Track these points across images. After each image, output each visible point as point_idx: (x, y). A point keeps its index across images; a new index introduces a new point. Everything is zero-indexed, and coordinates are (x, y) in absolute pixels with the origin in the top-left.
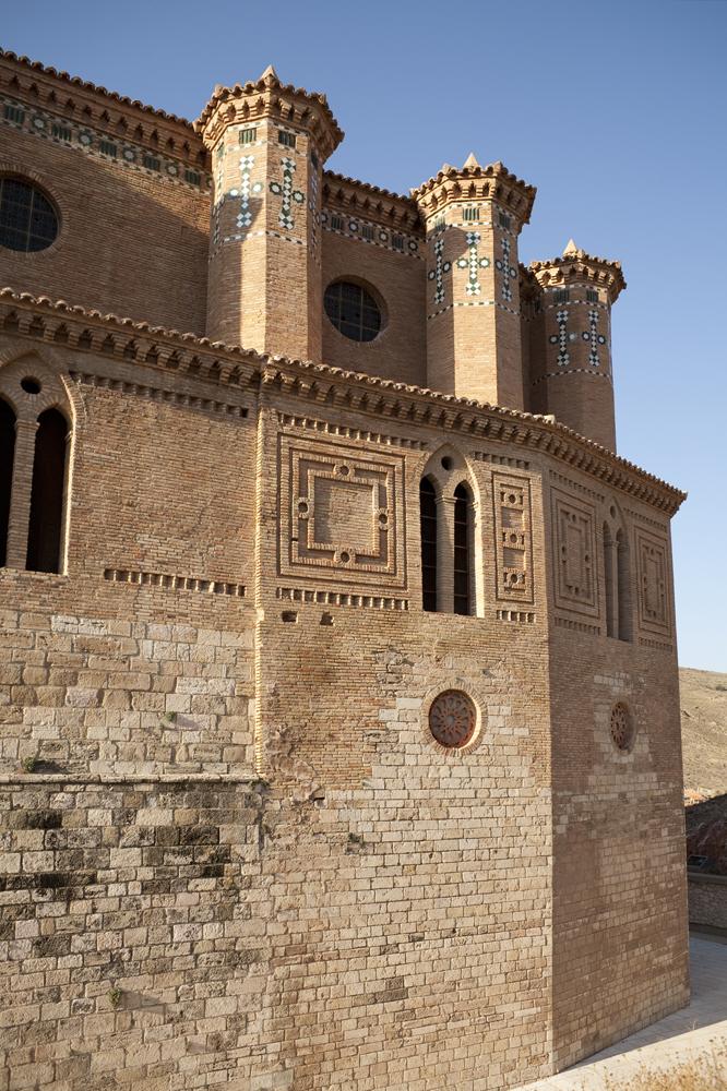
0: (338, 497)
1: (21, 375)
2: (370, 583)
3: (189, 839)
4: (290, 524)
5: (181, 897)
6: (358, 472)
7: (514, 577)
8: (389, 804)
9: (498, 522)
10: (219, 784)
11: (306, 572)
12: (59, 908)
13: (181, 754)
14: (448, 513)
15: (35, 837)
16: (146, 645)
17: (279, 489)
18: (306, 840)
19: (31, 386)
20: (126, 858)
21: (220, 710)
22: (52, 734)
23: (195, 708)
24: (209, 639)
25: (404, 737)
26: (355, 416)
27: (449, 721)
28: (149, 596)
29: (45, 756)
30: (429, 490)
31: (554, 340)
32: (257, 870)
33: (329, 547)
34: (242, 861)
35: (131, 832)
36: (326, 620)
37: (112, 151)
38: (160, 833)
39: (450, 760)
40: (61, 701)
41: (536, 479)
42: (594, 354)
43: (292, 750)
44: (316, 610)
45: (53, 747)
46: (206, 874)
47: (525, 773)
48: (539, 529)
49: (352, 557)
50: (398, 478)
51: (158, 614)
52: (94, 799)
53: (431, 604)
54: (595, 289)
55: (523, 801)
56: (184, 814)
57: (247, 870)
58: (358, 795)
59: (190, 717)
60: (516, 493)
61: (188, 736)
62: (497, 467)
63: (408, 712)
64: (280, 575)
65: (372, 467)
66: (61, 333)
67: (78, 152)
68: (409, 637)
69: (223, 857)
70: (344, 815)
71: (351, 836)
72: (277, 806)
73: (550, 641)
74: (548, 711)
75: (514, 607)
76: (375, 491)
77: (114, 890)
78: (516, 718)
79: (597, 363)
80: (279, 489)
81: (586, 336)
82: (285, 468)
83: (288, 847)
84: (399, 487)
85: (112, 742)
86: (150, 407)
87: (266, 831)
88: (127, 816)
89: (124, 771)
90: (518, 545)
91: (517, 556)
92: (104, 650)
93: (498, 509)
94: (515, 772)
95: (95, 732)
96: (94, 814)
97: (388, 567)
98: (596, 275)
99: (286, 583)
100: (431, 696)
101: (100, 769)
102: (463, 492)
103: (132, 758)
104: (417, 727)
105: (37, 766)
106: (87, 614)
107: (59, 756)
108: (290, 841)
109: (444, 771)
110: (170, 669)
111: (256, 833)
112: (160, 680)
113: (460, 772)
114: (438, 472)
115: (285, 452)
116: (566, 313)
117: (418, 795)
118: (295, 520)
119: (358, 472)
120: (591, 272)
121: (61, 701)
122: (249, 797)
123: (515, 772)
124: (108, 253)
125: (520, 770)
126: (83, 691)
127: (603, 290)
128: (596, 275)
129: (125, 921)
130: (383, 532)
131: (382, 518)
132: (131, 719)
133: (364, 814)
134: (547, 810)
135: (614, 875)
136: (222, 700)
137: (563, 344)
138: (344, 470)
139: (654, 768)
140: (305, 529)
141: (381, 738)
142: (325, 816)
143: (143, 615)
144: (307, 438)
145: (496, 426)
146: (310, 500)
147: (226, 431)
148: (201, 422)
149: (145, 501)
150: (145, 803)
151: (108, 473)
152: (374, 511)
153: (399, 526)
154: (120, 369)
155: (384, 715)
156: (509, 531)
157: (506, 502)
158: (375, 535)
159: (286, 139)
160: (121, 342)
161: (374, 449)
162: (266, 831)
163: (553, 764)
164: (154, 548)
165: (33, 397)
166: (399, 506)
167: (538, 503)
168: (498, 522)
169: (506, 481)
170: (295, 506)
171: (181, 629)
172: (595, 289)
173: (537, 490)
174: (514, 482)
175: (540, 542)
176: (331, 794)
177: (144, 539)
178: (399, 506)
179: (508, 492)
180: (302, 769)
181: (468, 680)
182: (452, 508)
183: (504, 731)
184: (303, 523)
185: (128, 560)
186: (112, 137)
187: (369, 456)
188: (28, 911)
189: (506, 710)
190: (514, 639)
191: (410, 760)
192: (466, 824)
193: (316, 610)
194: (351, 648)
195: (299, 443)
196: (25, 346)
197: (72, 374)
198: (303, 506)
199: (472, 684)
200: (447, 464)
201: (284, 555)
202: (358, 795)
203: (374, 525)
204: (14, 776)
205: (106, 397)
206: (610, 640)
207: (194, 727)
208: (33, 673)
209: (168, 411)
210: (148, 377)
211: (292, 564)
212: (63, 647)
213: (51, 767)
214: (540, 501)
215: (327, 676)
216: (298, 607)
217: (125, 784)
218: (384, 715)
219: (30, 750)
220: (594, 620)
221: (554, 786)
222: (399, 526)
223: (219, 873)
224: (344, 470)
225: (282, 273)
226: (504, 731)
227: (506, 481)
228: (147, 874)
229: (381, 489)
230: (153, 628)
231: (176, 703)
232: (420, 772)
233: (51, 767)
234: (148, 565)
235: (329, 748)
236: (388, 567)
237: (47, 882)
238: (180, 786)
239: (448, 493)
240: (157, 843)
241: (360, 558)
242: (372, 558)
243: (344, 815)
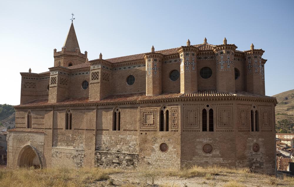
0: (148, 116)
2: (152, 128)
3: (130, 160)
5: (130, 167)
7: (175, 125)
8: (154, 159)
9: (172, 116)
11: (144, 127)
13: (131, 151)
14: (165, 115)
15: (117, 159)
16: (127, 138)
20: (124, 162)
21: (135, 146)
22: (119, 148)
23: (132, 145)
25: (156, 150)
26: (150, 104)
27: (163, 148)
28: (128, 132)
29: (119, 150)
30: (162, 113)
31: (224, 62)
32: (137, 165)
33: (147, 124)
34: (136, 164)
35: (125, 159)
36: (146, 134)
37: (139, 66)
38: (128, 159)
40: (120, 144)
41: (179, 107)
42: (229, 66)
45: (119, 149)
46: (132, 165)
47: (176, 156)
48: (180, 115)
51: (129, 134)
52: (122, 155)
53: (162, 129)
54: (222, 51)
55: (175, 161)
57: (136, 165)
58: (149, 157)
59: (131, 146)
60: (175, 110)
61: (132, 149)
63: (157, 146)
64: (140, 128)
65: (152, 111)
67: (136, 69)
68: (157, 135)
69: (134, 163)
70: (148, 160)
71: (148, 163)
72: (140, 158)
73: (181, 135)
74: (180, 146)
75: (174, 129)
77: (124, 165)
78: (174, 148)
79: (229, 68)
81: (227, 62)
84: (156, 113)
86: (127, 110)
87: (138, 161)
88: (124, 157)
89: (125, 152)
90: (176, 119)
91: (176, 121)
93: (172, 114)
94: (174, 156)
96: (122, 157)
98: (221, 48)
99: (141, 129)
100: (160, 144)
101: (123, 152)
102: (167, 111)
104: (158, 148)
105: (118, 151)
106: (122, 135)
108: (141, 162)
109: (162, 155)
110: (130, 141)
113: (164, 155)
114: (163, 109)
116: (223, 57)
117: (158, 158)
120: (220, 48)
121: (120, 144)
122: (137, 156)
123: (174, 156)
124: (140, 81)
125: (175, 156)
126: (122, 143)
127: (224, 51)
128: (221, 48)
129: (124, 169)
130: (154, 120)
131: (154, 118)
132: (126, 146)
133: (150, 160)
134: (179, 163)
135: (41, 142)
137: (222, 64)
138: (149, 113)
139: (221, 157)
140: (144, 122)
141: (153, 150)
144: (143, 109)
145: (170, 100)
146: (144, 118)
147: (135, 110)
148: (132, 110)
149: (127, 121)
151: (124, 118)
152: (153, 117)
153: (156, 119)
155: (153, 147)
156: (174, 117)
157: (174, 112)
158: (153, 121)
160: (123, 103)
161: (152, 109)
162: (138, 161)
163: (181, 155)
167: (180, 111)
168: (172, 116)
169: (173, 108)
171: (131, 136)
172: (222, 51)
173: (179, 109)
174: (175, 108)
175: (180, 118)
176: (146, 157)
178: (156, 116)
179: (174, 110)
181: (166, 141)
183: (172, 149)
185: (126, 128)
186: (140, 64)
187: (152, 110)
189: (172, 146)
191: (157, 153)
192: (165, 163)
194: (149, 137)
196: (116, 106)
197: (120, 108)
198: (143, 119)
199: (167, 142)
200: (165, 108)
202: (149, 157)
203: (153, 120)
204: (116, 152)
206: (205, 133)
208: (118, 141)
209: (129, 110)
212: (120, 139)
213: (119, 151)
214: (180, 111)
215: (146, 141)
217: (124, 154)
218: (153, 147)
220: (216, 127)
221: (181, 159)
222: (156, 119)
223: (133, 165)
224: (149, 113)
226: (172, 149)
227: (173, 108)
228: (126, 164)
229: (154, 114)
231: (130, 145)
232: (158, 155)
233: (119, 151)
234: (127, 129)
235: (146, 151)
238: (130, 154)
239: (165, 112)
240: (128, 161)
241: (150, 125)
243: (148, 160)
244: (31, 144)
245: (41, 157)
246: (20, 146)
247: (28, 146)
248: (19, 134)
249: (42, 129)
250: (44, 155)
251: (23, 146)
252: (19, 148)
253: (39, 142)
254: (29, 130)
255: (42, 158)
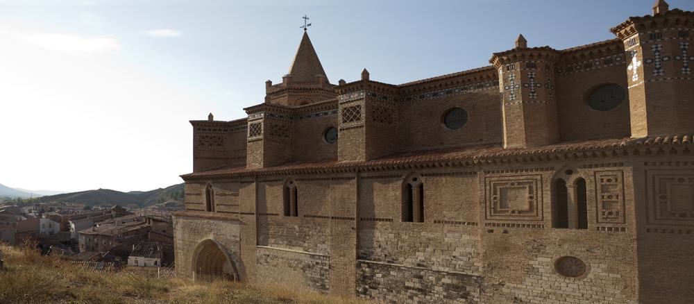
0: (511, 194)
1: (412, 178)
3: (456, 287)
4: (490, 204)
6: (519, 184)
10: (466, 275)
11: (497, 218)
12: (423, 296)
13: (457, 266)
16: (446, 239)
17: (486, 194)
18: (496, 296)
19: (415, 179)
23: (462, 255)
24: (466, 238)
28: (447, 227)
29: (421, 263)
36: (506, 232)
37: (482, 86)
39: (567, 281)
43: (492, 269)
44: (501, 229)
45: (423, 261)
46: (462, 297)
49: (517, 212)
50: (539, 183)
51: (449, 231)
56: (455, 281)
61: (459, 262)
62: (596, 169)
66: (416, 167)
73: (637, 239)
76: (528, 188)
80: (486, 194)
82: (488, 187)
83: (490, 296)
85: (438, 262)
86: (444, 179)
88: (438, 279)
92: (434, 240)
95: (433, 259)
96: (430, 277)
97: (535, 214)
99: (489, 222)
102: (581, 184)
103: (443, 266)
104: (549, 268)
105: (419, 265)
107: (425, 264)
108: (491, 294)
111: (478, 291)
112: (449, 248)
115: (488, 183)
118: (492, 202)
119: (519, 184)
126: (430, 249)
131: (531, 198)
135: (234, 236)
136: (471, 254)
142: (505, 290)
143: (445, 231)
144: (495, 178)
150: (444, 276)
151: (433, 197)
152: (527, 195)
154: (434, 171)
159: (530, 66)
164: (448, 214)
165: (415, 182)
166: (539, 192)
170: (492, 198)
173: (629, 178)
176: (507, 284)
177: (444, 212)
178: (539, 192)
180: (496, 275)
182: (572, 189)
184: (495, 204)
188: (416, 295)
190: (610, 238)
193: (501, 229)
195: (493, 179)
198: (495, 198)
201: (488, 213)
205: (430, 179)
207: (461, 260)
208: (418, 245)
209: (449, 178)
210: (443, 171)
211: (491, 215)
213: (423, 266)
216: (495, 229)
217: (438, 272)
219: (418, 261)
222: (540, 199)
225: (512, 116)
230: (448, 235)
233: (423, 266)
234: (446, 219)
236: (492, 214)
237: (419, 290)
238: (454, 275)
240: (447, 287)
242: (527, 211)
243: (513, 291)
244: (216, 239)
245: (235, 261)
246: (196, 241)
247: (210, 240)
248: (192, 221)
249: (235, 215)
250: (240, 259)
251: (200, 241)
252: (194, 242)
253: (230, 236)
254: (211, 214)
255: (237, 264)
